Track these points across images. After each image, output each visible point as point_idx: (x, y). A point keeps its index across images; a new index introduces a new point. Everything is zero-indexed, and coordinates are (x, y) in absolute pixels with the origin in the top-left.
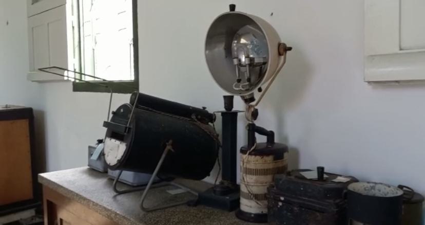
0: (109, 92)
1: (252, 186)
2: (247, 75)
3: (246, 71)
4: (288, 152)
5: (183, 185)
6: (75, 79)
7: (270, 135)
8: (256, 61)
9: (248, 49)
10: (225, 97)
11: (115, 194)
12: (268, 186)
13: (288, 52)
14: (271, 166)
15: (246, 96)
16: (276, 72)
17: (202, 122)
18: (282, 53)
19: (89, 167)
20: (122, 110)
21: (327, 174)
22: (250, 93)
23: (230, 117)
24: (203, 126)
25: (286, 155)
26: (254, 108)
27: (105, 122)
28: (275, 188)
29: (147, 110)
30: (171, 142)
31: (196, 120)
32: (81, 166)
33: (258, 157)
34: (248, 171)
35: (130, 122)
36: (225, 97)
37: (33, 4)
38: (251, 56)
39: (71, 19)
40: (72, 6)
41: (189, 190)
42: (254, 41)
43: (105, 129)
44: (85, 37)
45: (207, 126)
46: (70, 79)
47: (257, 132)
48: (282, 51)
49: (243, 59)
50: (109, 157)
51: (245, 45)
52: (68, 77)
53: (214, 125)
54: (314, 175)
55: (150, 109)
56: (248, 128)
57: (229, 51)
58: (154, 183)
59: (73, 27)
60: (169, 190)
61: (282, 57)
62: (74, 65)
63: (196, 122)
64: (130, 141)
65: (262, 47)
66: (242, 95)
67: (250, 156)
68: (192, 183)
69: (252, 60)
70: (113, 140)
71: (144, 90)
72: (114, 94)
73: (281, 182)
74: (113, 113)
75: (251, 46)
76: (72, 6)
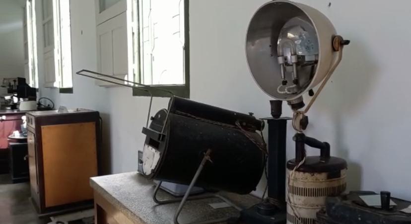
0: (150, 96)
1: (300, 208)
2: (294, 76)
3: (293, 72)
4: (347, 169)
5: (228, 199)
6: (135, 83)
7: (325, 148)
8: (307, 59)
9: (296, 45)
10: (271, 102)
11: (155, 204)
12: (318, 210)
13: (345, 46)
14: (324, 186)
15: (292, 101)
16: (329, 72)
17: (248, 130)
18: (336, 49)
19: (138, 172)
20: (159, 116)
21: (395, 200)
22: (299, 96)
23: (278, 125)
24: (248, 134)
25: (343, 172)
26: (303, 116)
27: (144, 128)
28: (326, 215)
29: (186, 116)
30: (209, 151)
31: (240, 127)
32: (129, 171)
33: (307, 175)
34: (296, 191)
35: (164, 130)
36: (271, 102)
37: (100, 12)
38: (300, 53)
39: (131, 25)
40: (132, 13)
41: (233, 205)
42: (303, 35)
43: (145, 136)
44: (144, 43)
45: (253, 133)
46: (130, 83)
47: (307, 144)
48: (336, 45)
49: (289, 56)
50: (146, 166)
51: (293, 40)
52: (128, 81)
53: (261, 133)
54: (375, 201)
55: (189, 115)
56: (295, 139)
57: (274, 46)
58: (190, 195)
59: (133, 33)
60: (212, 203)
61: (338, 53)
62: (134, 70)
63: (240, 129)
64: (164, 148)
65: (312, 43)
66: (287, 99)
67: (297, 173)
68: (238, 197)
69: (299, 57)
70: (150, 148)
71: (197, 96)
72: (153, 98)
73: (333, 208)
74: (152, 118)
75: (300, 41)
76: (132, 13)
